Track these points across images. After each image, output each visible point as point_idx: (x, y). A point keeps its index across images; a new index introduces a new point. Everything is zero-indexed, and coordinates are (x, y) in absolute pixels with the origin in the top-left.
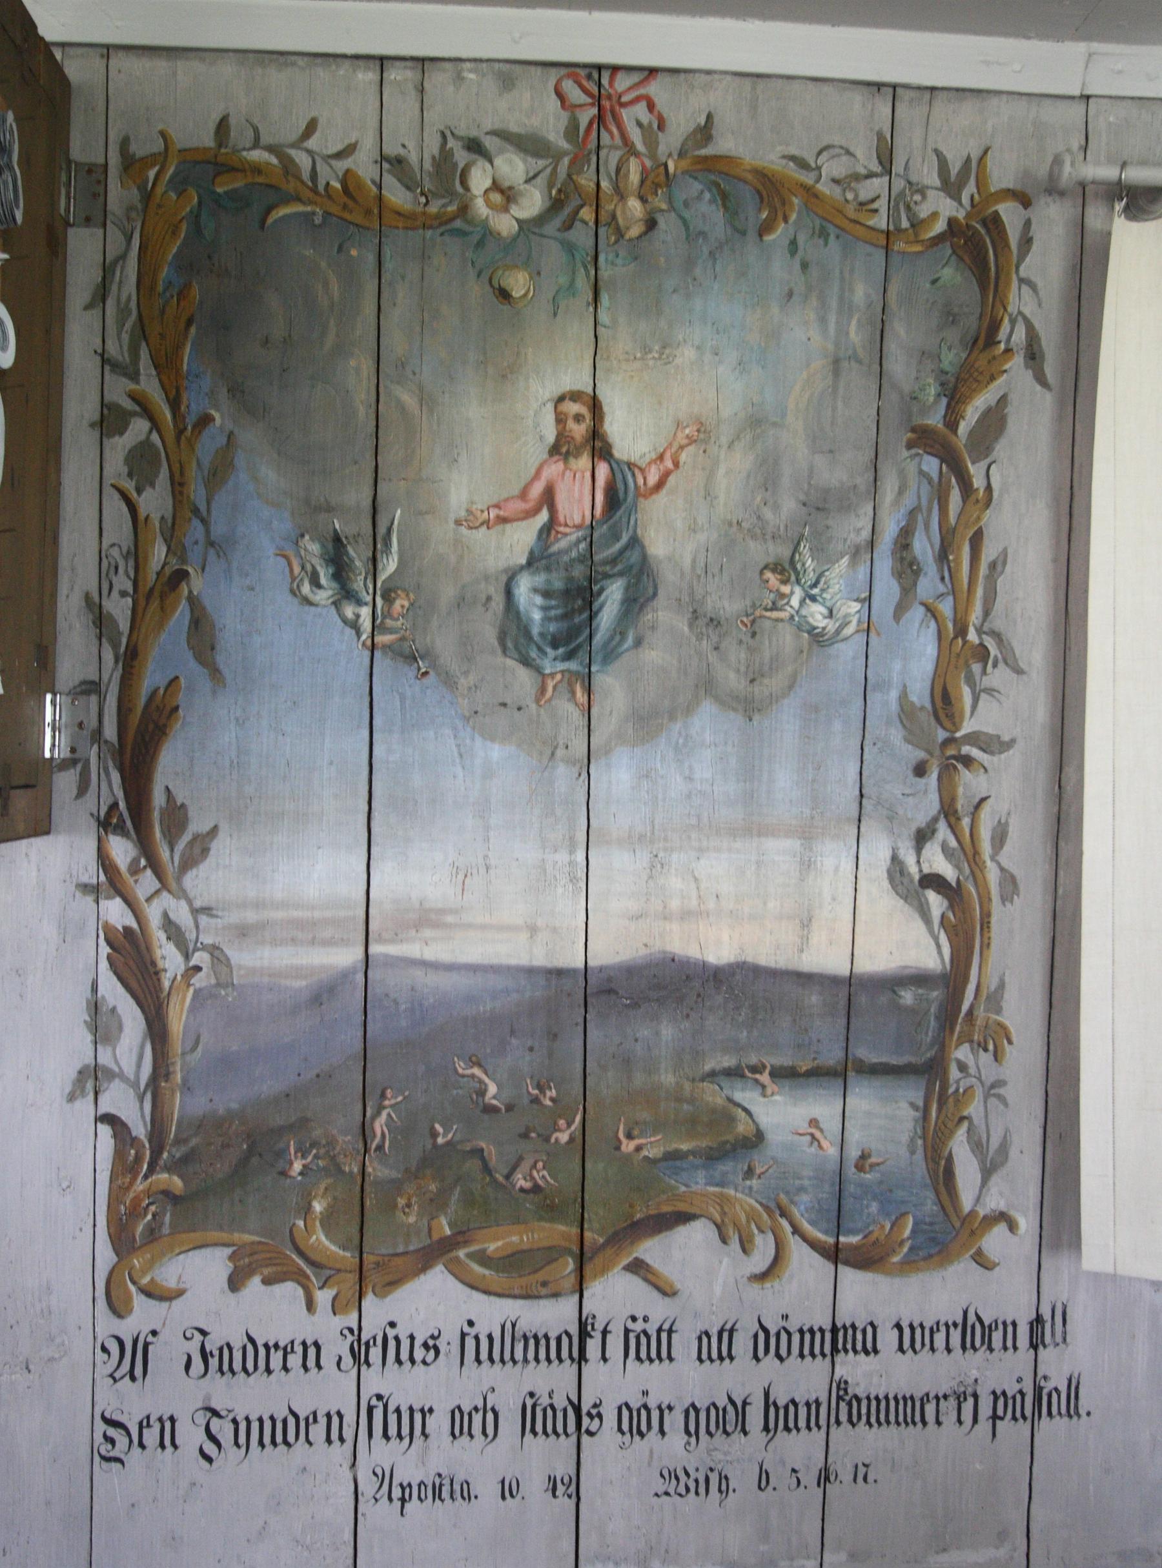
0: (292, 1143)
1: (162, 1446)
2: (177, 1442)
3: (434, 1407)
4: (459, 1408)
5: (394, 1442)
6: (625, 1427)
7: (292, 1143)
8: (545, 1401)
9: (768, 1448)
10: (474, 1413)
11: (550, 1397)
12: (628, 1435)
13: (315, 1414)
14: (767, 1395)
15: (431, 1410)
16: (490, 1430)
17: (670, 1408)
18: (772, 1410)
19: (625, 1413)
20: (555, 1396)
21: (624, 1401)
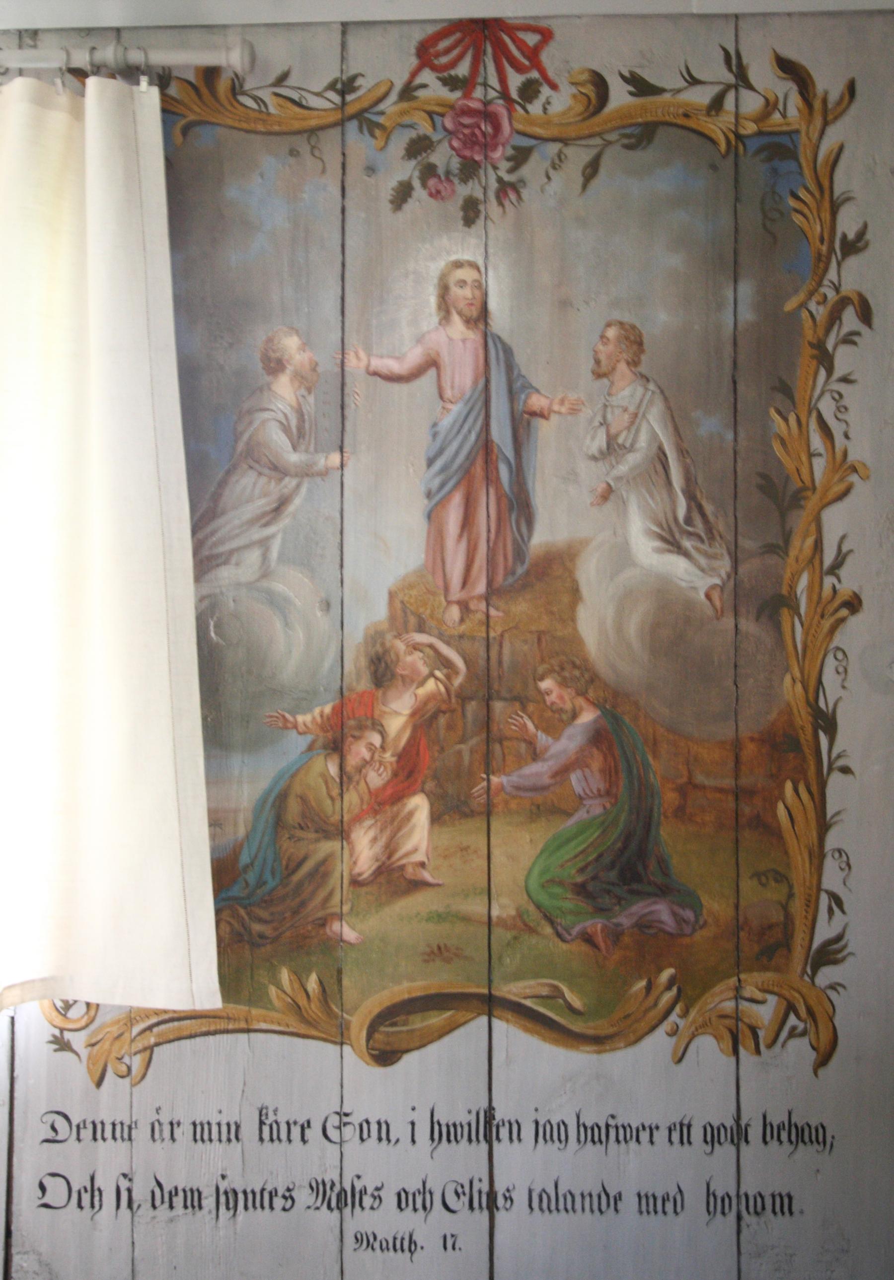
0: (224, 643)
1: (95, 1139)
2: (522, 1137)
3: (659, 1125)
4: (549, 1122)
5: (598, 1145)
6: (709, 1138)
7: (224, 643)
8: (271, 1118)
9: (435, 1155)
10: (417, 1194)
11: (275, 1114)
12: (822, 1145)
13: (84, 1122)
14: (765, 1117)
15: (657, 1128)
16: (563, 1137)
17: (179, 1124)
18: (582, 1130)
19: (403, 1195)
20: (279, 1113)
21: (364, 1118)
